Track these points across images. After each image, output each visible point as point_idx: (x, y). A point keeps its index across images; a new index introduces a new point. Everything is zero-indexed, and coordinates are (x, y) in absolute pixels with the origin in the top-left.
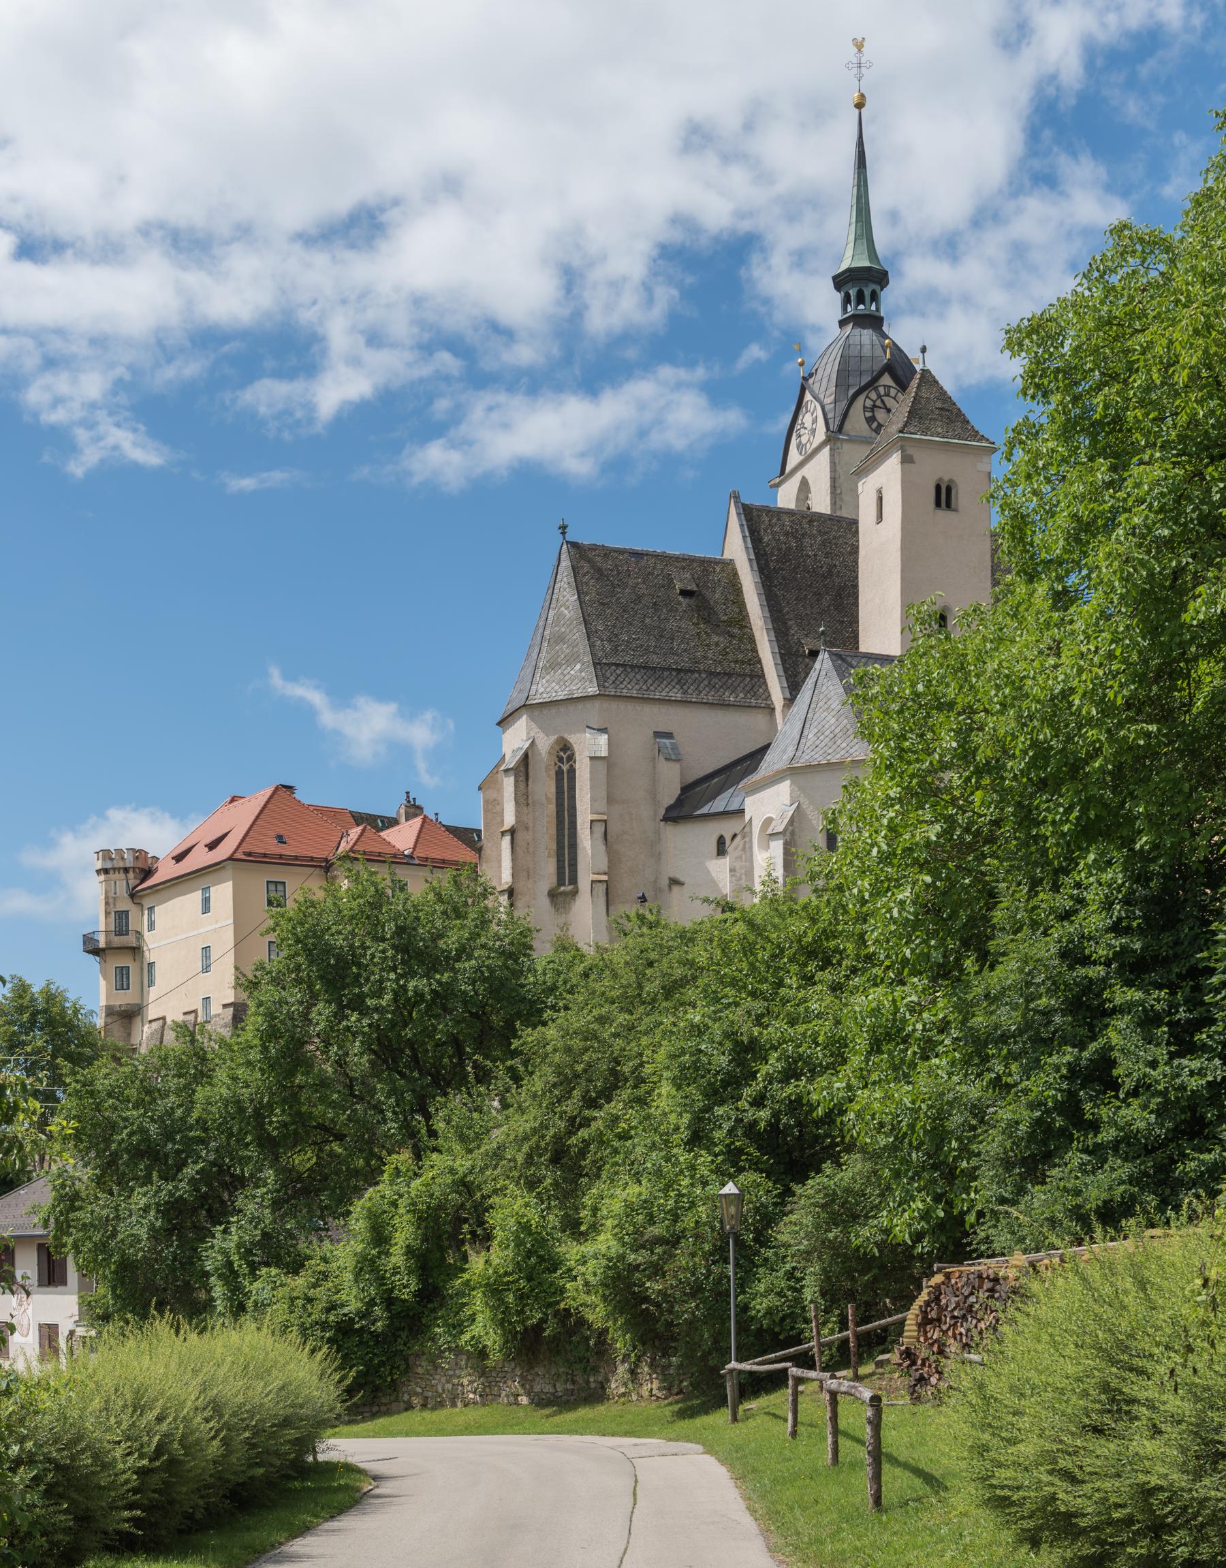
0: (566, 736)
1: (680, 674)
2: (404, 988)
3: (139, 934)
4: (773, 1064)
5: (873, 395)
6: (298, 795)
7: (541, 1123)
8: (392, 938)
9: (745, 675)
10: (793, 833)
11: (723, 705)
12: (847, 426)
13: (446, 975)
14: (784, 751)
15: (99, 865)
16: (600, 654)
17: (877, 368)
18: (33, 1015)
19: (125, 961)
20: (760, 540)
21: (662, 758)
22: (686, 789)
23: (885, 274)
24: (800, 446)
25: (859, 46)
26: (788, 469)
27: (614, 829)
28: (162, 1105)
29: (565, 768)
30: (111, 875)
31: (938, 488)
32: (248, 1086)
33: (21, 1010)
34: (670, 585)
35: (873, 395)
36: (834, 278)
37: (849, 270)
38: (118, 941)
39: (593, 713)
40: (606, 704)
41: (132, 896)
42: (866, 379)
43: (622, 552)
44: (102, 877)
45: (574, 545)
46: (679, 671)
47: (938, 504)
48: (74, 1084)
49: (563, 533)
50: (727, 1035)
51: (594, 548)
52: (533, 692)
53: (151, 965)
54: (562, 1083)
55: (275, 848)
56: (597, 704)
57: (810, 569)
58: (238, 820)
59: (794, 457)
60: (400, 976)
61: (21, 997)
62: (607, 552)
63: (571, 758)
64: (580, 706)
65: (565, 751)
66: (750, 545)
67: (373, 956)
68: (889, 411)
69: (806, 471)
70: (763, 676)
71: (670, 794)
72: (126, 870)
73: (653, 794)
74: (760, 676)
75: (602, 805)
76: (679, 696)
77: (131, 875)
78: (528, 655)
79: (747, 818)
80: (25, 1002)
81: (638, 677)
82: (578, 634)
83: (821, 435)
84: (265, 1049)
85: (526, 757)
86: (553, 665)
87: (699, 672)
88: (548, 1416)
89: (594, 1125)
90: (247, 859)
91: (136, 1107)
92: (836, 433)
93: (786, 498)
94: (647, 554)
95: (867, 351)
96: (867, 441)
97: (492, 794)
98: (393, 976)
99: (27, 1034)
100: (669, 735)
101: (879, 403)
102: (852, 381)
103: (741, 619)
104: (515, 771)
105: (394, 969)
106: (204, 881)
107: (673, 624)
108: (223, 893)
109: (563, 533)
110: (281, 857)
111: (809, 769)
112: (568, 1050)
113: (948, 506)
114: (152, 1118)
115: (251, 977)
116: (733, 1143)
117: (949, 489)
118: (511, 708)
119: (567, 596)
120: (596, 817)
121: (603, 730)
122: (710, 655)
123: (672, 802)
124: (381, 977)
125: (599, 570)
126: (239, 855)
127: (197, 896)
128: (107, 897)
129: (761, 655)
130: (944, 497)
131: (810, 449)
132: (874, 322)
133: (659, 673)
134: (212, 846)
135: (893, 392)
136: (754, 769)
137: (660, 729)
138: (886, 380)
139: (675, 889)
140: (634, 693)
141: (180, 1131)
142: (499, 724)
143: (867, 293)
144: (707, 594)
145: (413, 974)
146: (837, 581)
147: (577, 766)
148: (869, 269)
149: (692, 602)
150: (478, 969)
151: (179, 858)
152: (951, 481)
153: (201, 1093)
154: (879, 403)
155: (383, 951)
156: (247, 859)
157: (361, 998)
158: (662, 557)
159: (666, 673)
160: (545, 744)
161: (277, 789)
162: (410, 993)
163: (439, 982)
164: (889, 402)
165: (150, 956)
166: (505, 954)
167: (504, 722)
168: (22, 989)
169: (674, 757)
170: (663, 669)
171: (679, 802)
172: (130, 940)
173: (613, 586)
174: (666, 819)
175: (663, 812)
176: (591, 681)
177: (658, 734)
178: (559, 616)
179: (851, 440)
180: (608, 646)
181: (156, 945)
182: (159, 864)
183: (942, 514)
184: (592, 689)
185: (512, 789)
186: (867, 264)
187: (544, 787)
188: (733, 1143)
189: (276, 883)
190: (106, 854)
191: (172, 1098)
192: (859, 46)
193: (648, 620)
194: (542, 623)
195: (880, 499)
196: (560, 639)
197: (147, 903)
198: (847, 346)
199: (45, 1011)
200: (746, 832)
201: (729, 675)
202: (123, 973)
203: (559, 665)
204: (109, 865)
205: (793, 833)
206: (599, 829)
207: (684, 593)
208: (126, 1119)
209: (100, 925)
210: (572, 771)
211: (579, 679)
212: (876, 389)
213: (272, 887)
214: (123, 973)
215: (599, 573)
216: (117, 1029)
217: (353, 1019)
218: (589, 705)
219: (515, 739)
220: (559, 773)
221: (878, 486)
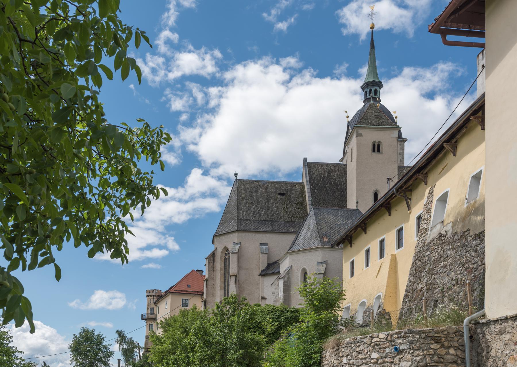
10: (289, 278)
30: (150, 297)
40: (240, 234)
41: (155, 303)
47: (374, 151)
49: (236, 177)
55: (186, 288)
66: (308, 176)
72: (154, 296)
77: (155, 297)
81: (255, 224)
100: (266, 244)
109: (236, 177)
123: (264, 269)
137: (263, 242)
143: (373, 90)
148: (374, 81)
152: (379, 142)
170: (266, 221)
174: (260, 275)
190: (149, 291)
193: (264, 204)
202: (152, 325)
213: (184, 301)
220: (225, 259)
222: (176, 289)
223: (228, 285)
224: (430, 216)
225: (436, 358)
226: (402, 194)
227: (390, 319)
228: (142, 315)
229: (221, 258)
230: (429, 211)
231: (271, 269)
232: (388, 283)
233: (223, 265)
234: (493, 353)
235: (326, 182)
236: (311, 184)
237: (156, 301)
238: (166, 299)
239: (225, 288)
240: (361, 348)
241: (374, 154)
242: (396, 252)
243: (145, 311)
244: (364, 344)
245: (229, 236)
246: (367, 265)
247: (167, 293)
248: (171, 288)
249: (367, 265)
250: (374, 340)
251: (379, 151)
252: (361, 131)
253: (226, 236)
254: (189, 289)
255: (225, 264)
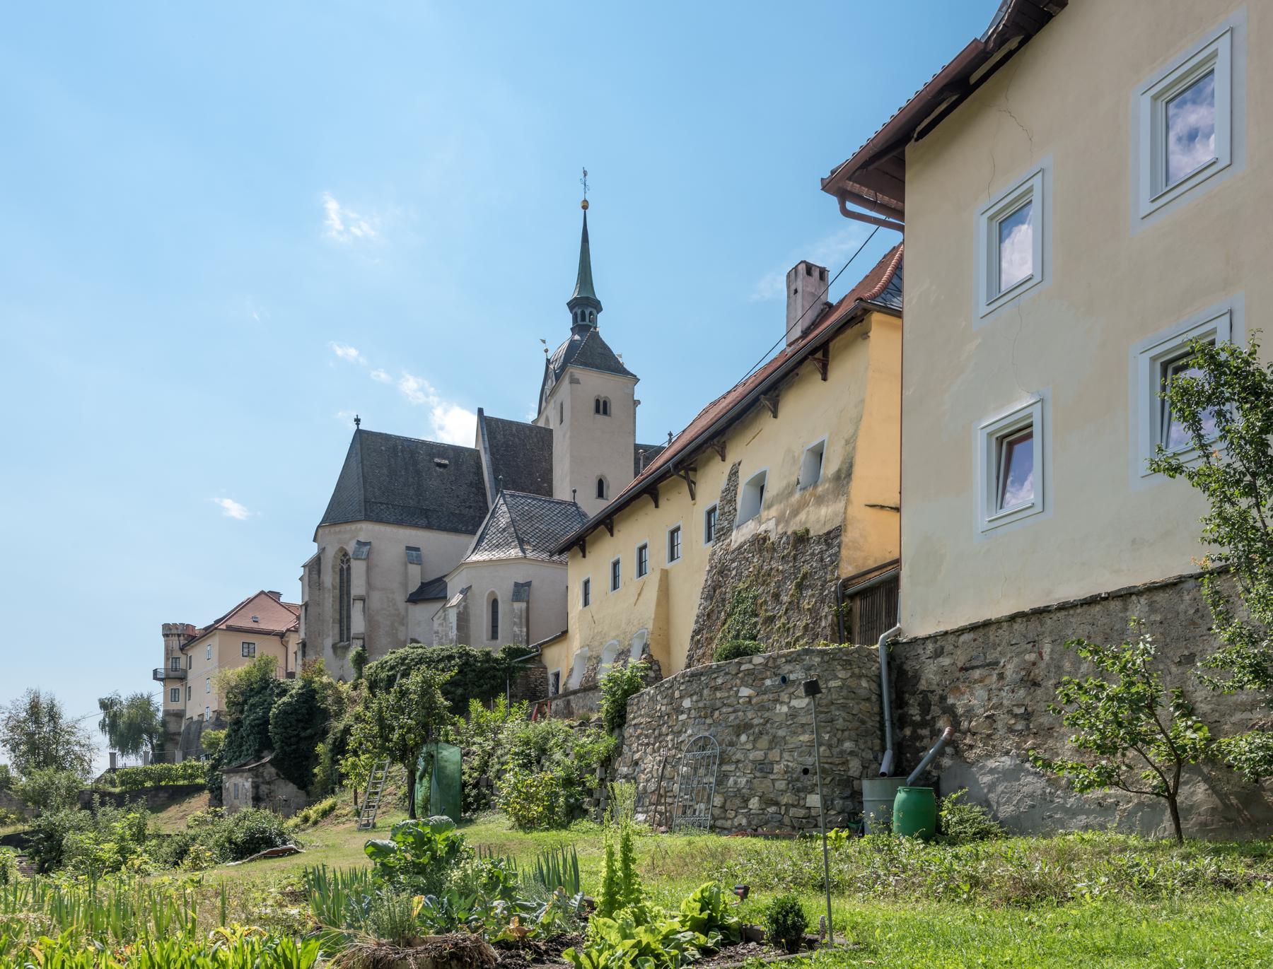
6: (282, 600)
19: (177, 685)
47: (597, 411)
55: (247, 624)
71: (414, 587)
73: (405, 585)
88: (611, 854)
100: (417, 549)
143: (587, 313)
166: (261, 679)
177: (408, 548)
183: (600, 417)
202: (175, 691)
209: (160, 664)
214: (175, 691)
220: (341, 570)
222: (229, 623)
223: (349, 617)
224: (735, 510)
225: (844, 693)
226: (682, 473)
227: (660, 670)
228: (155, 672)
229: (333, 567)
230: (732, 501)
231: (431, 591)
232: (656, 614)
233: (338, 580)
234: (923, 685)
235: (516, 454)
236: (492, 454)
237: (185, 646)
238: (210, 641)
239: (341, 622)
240: (720, 681)
241: (598, 416)
242: (668, 566)
244: (727, 674)
246: (615, 587)
247: (209, 631)
248: (217, 622)
249: (615, 587)
250: (743, 668)
251: (605, 412)
254: (254, 626)
255: (341, 580)
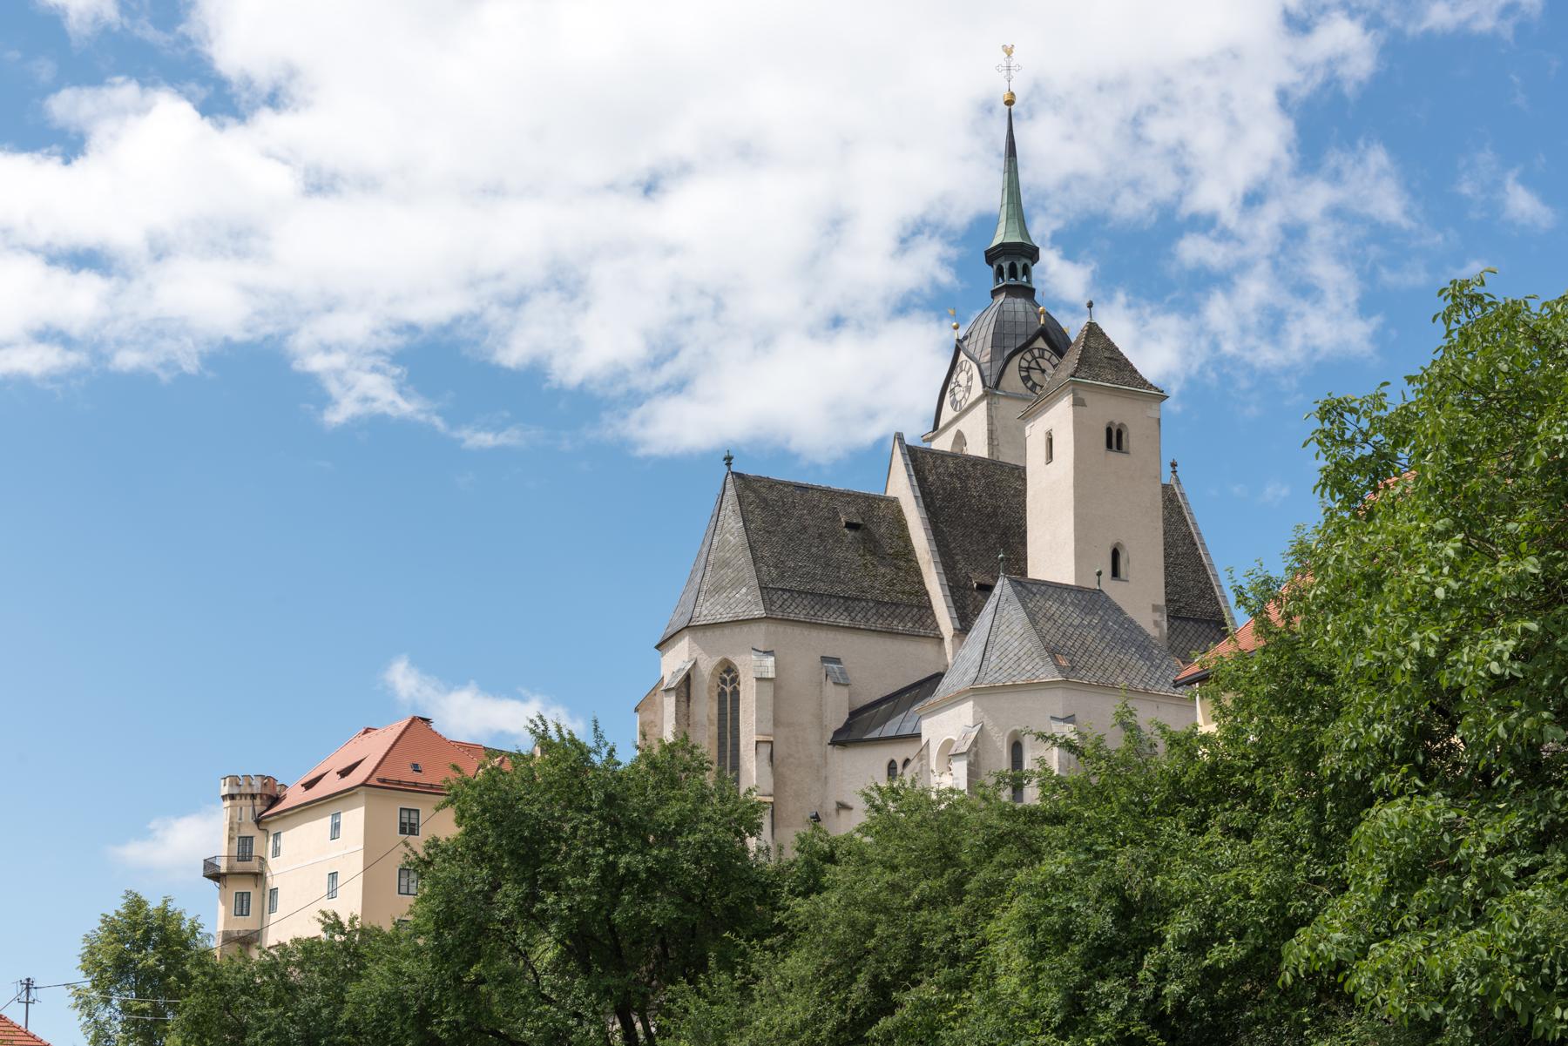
0: (730, 658)
1: (848, 602)
2: (613, 866)
3: (262, 860)
4: (1181, 924)
5: (1028, 357)
7: (815, 1015)
8: (600, 808)
9: (912, 606)
10: (976, 754)
11: (892, 633)
12: (1003, 384)
13: (665, 851)
14: (965, 674)
15: (225, 791)
16: (766, 578)
17: (1032, 332)
18: (148, 932)
20: (926, 479)
21: (830, 682)
22: (854, 714)
23: (1037, 250)
24: (954, 403)
25: (1009, 51)
26: (941, 425)
27: (780, 750)
28: (305, 1002)
29: (728, 689)
30: (237, 801)
31: (1109, 431)
32: (413, 981)
33: (134, 927)
34: (835, 517)
35: (1028, 357)
36: (987, 253)
37: (1002, 245)
38: (240, 866)
39: (759, 635)
40: (772, 627)
41: (259, 821)
42: (1020, 342)
43: (787, 484)
44: (228, 803)
45: (739, 476)
46: (846, 599)
47: (1109, 445)
48: (201, 978)
49: (729, 464)
50: (1107, 891)
51: (759, 479)
52: (696, 613)
53: (274, 891)
54: (839, 966)
55: (409, 776)
56: (763, 627)
57: (977, 509)
58: (372, 750)
59: (948, 413)
60: (608, 852)
61: (135, 913)
62: (772, 484)
63: (735, 680)
64: (745, 629)
65: (728, 673)
67: (575, 828)
68: (1043, 371)
69: (961, 425)
70: (931, 607)
71: (837, 718)
72: (253, 796)
73: (820, 718)
74: (927, 607)
75: (769, 727)
76: (847, 623)
77: (258, 801)
78: (690, 580)
79: (924, 741)
80: (140, 918)
82: (744, 559)
83: (978, 390)
84: (438, 936)
85: (688, 678)
86: (717, 589)
87: (867, 601)
89: (899, 1013)
90: (380, 785)
91: (274, 1005)
92: (993, 389)
93: (943, 443)
94: (812, 488)
95: (1021, 317)
96: (1023, 399)
97: (649, 716)
98: (600, 851)
99: (139, 952)
100: (837, 661)
101: (1033, 364)
102: (1007, 342)
103: (908, 552)
104: (677, 690)
105: (601, 843)
106: (335, 808)
107: (839, 554)
108: (354, 819)
109: (729, 464)
110: (416, 784)
111: (993, 689)
112: (852, 924)
113: (1119, 448)
114: (292, 1021)
115: (422, 854)
116: (1127, 1029)
117: (1119, 433)
118: (671, 631)
119: (733, 524)
120: (761, 738)
121: (768, 653)
122: (877, 585)
124: (586, 852)
125: (765, 500)
126: (373, 781)
127: (326, 823)
128: (231, 823)
129: (928, 587)
130: (1115, 439)
131: (965, 405)
132: (1028, 292)
133: (825, 600)
134: (344, 773)
135: (1047, 355)
136: (931, 692)
138: (1041, 343)
139: (843, 813)
140: (802, 617)
141: (326, 1034)
142: (658, 647)
143: (1019, 267)
144: (873, 528)
145: (622, 849)
146: (1002, 522)
147: (741, 688)
148: (1021, 244)
149: (858, 534)
150: (703, 845)
151: (309, 785)
152: (1121, 425)
153: (353, 990)
154: (1033, 364)
155: (589, 823)
156: (380, 785)
157: (559, 875)
158: (827, 492)
159: (833, 600)
160: (708, 665)
161: (414, 720)
162: (622, 871)
163: (656, 859)
164: (1044, 364)
165: (272, 882)
167: (662, 645)
168: (136, 905)
169: (842, 682)
170: (830, 596)
171: (848, 727)
172: (254, 866)
173: (779, 516)
174: (833, 743)
175: (831, 735)
176: (757, 604)
177: (824, 659)
178: (723, 543)
179: (1007, 396)
180: (774, 573)
181: (279, 871)
182: (288, 792)
183: (1113, 455)
184: (759, 612)
185: (673, 709)
186: (1019, 240)
187: (705, 708)
188: (1127, 1029)
189: (410, 810)
190: (234, 780)
191: (319, 996)
192: (1009, 51)
193: (814, 550)
194: (705, 549)
195: (1050, 441)
196: (725, 564)
197: (273, 829)
198: (1001, 311)
199: (161, 928)
200: (922, 754)
201: (897, 605)
203: (724, 589)
204: (235, 791)
205: (976, 754)
206: (765, 750)
207: (850, 526)
208: (261, 1019)
210: (736, 694)
211: (745, 600)
212: (1031, 351)
213: (405, 814)
215: (765, 504)
216: (233, 949)
217: (550, 900)
218: (754, 627)
219: (675, 662)
220: (722, 694)
221: (1047, 428)
243: (220, 847)
245: (737, 630)
252: (1081, 394)
253: (727, 631)
